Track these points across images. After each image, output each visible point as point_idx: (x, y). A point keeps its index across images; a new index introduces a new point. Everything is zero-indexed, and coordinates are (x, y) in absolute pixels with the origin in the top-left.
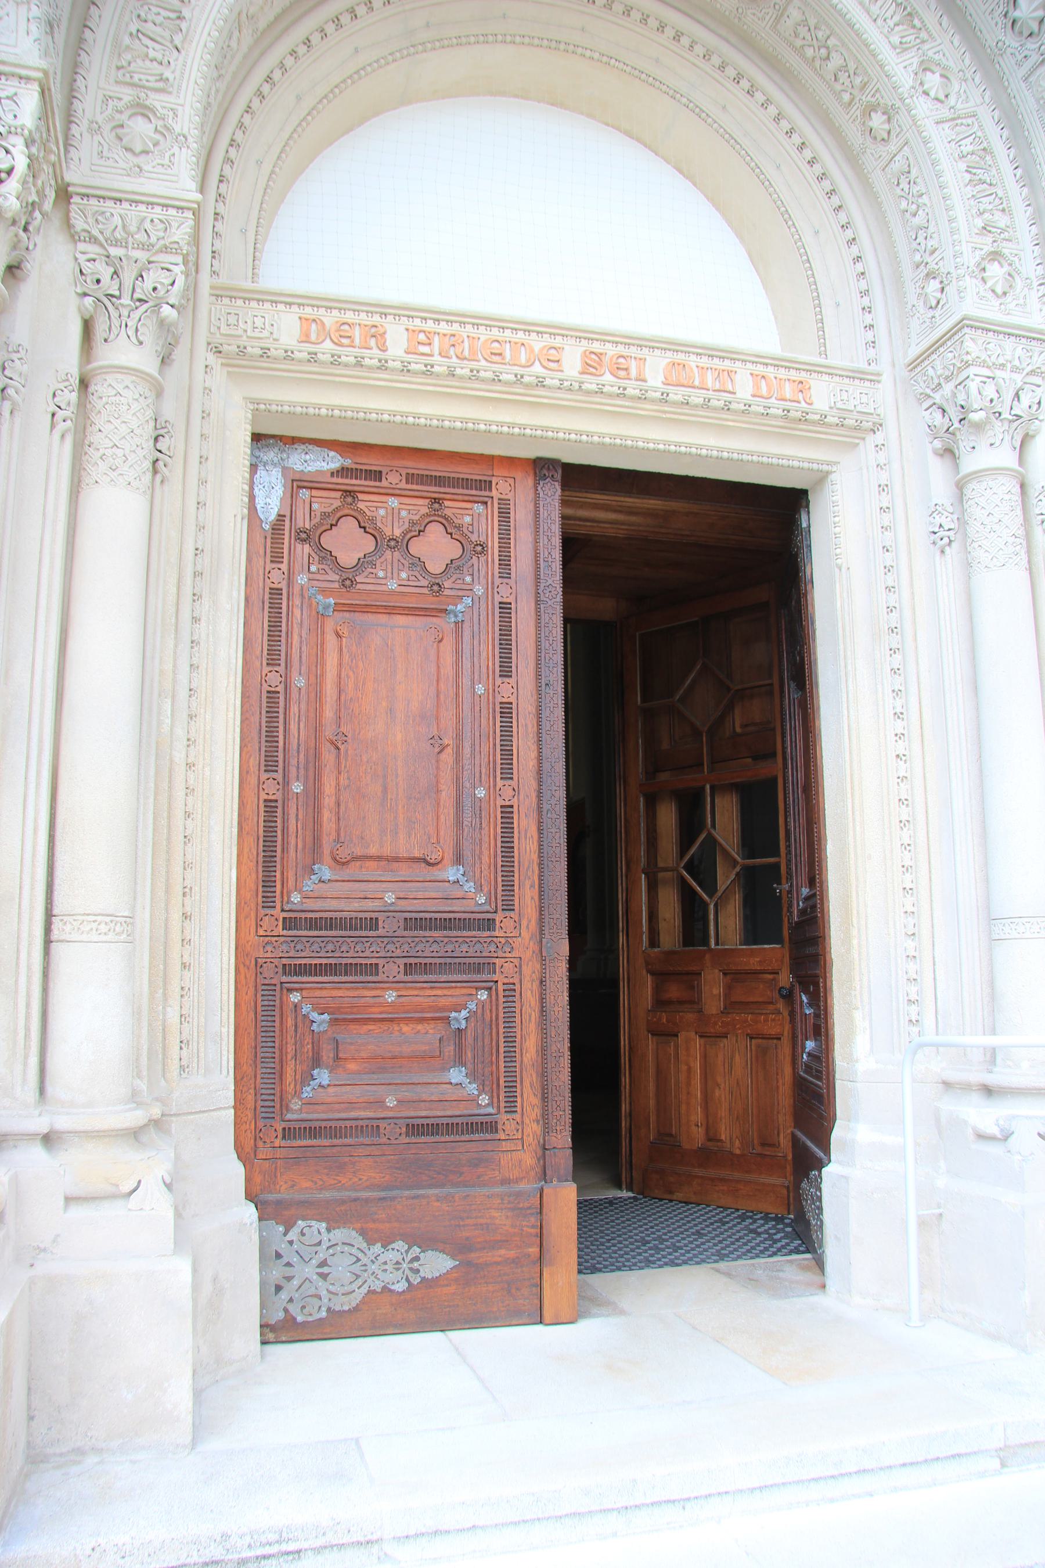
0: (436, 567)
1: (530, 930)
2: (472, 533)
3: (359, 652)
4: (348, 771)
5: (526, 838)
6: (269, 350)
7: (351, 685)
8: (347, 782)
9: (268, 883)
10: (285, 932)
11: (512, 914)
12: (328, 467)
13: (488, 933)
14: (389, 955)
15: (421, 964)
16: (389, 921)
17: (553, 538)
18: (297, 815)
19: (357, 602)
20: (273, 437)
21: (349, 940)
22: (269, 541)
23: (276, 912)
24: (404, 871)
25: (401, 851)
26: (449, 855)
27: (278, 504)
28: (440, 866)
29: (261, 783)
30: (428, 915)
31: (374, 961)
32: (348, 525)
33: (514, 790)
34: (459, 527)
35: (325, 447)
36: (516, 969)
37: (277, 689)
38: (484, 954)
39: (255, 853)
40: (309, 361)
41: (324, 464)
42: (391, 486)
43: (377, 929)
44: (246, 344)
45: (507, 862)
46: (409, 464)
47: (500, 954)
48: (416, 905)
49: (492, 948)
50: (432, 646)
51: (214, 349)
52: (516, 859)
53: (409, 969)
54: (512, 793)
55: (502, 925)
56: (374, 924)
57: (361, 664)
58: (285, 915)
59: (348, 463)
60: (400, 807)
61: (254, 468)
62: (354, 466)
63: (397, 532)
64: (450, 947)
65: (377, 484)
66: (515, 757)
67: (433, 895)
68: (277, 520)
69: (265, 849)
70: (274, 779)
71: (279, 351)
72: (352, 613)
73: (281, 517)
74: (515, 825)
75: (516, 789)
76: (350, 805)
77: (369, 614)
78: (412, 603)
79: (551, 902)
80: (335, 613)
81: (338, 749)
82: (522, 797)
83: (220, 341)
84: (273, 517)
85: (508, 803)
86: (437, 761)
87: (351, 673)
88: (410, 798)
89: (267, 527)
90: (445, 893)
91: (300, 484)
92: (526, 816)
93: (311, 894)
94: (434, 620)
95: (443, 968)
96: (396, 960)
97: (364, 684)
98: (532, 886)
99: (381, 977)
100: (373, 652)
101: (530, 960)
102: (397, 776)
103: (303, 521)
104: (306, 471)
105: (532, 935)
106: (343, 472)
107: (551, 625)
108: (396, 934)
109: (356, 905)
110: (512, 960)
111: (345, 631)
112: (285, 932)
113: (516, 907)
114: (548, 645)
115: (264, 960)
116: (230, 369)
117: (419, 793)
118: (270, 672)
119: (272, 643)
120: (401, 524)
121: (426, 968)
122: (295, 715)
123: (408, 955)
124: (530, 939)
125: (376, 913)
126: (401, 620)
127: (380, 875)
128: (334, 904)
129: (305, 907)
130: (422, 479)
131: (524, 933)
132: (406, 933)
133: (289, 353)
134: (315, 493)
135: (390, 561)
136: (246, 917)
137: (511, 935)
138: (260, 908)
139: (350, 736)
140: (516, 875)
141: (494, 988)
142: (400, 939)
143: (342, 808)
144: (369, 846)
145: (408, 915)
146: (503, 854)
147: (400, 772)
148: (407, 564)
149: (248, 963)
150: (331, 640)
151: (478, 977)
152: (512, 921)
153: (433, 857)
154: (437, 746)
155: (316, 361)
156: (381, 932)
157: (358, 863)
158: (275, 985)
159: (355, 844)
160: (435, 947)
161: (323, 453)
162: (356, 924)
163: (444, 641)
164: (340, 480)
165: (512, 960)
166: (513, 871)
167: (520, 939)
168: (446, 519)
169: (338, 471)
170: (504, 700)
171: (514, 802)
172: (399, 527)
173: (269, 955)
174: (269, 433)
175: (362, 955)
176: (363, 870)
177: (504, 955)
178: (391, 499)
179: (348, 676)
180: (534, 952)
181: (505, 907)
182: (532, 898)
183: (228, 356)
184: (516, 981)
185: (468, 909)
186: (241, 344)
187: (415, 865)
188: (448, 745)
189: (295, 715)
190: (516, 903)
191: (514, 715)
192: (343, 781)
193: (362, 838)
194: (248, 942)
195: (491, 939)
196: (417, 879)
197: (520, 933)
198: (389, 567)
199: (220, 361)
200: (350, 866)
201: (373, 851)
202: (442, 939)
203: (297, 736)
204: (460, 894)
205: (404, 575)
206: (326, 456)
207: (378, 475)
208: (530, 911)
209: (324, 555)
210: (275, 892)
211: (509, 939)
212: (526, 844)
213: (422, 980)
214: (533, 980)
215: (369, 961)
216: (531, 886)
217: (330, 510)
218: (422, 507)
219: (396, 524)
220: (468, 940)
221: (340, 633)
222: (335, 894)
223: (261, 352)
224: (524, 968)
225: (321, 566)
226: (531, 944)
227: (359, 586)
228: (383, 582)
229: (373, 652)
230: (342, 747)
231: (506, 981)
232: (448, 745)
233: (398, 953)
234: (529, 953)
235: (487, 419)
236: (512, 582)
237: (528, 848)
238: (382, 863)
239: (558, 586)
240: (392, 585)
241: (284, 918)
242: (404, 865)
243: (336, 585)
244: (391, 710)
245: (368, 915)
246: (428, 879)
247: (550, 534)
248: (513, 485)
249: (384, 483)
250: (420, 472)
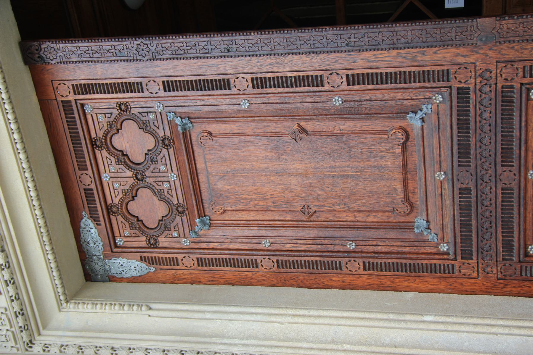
0: (150, 142)
1: (468, 54)
2: (111, 114)
3: (233, 197)
4: (333, 205)
5: (377, 61)
6: (16, 312)
7: (262, 203)
8: (342, 206)
9: (432, 269)
10: (474, 257)
11: (452, 72)
12: (94, 228)
13: (472, 96)
14: (493, 180)
15: (502, 153)
16: (462, 180)
17: (93, 48)
18: (374, 245)
19: (194, 201)
20: (83, 265)
21: (480, 211)
22: (162, 267)
23: (457, 264)
24: (415, 158)
25: (397, 163)
26: (399, 123)
27: (133, 261)
28: (408, 129)
29: (351, 272)
30: (455, 147)
31: (499, 191)
32: (134, 207)
33: (331, 74)
34: (110, 125)
35: (79, 231)
36: (509, 66)
37: (275, 261)
38: (493, 96)
39: (408, 278)
40: (14, 283)
41: (93, 231)
42: (93, 181)
43: (468, 88)
44: (17, 328)
45: (400, 78)
46: (71, 168)
47: (493, 81)
48: (446, 153)
49: (487, 89)
50: (216, 141)
51: (30, 345)
52: (397, 70)
53: (507, 162)
54: (334, 76)
55: (463, 81)
56: (464, 192)
57: (243, 196)
58: (459, 257)
59: (85, 214)
60: (359, 164)
61: (112, 279)
62: (87, 209)
63: (129, 173)
64: (486, 128)
65: (95, 191)
66: (302, 74)
67: (435, 140)
68: (146, 261)
69: (404, 270)
70: (347, 264)
71: (14, 306)
72: (204, 201)
73: (142, 259)
74: (365, 71)
75: (330, 72)
76: (361, 203)
77: (202, 189)
78: (184, 160)
79: (439, 39)
80: (206, 213)
81: (315, 212)
82: (337, 67)
83: (22, 344)
84: (144, 265)
85: (345, 79)
86: (315, 135)
87: (252, 203)
88: (350, 156)
89: (153, 269)
90: (434, 129)
91: (113, 247)
92: (354, 62)
93: (440, 236)
94: (194, 138)
95: (507, 133)
96: (498, 174)
97: (259, 193)
98: (423, 54)
99: (514, 185)
100: (232, 187)
101: (500, 52)
102: (331, 167)
103: (142, 241)
104: (102, 243)
105: (473, 52)
106: (94, 217)
107: (173, 49)
108: (474, 173)
109: (448, 202)
110: (499, 71)
111: (220, 208)
112: (474, 257)
113: (445, 68)
114: (192, 51)
115: (499, 273)
116: (41, 328)
117: (344, 149)
118: (262, 266)
119: (240, 264)
120: (121, 171)
121: (507, 148)
122: (293, 247)
123: (493, 164)
124: (477, 53)
125: (455, 189)
126: (200, 165)
127: (420, 180)
128: (448, 219)
129: (451, 240)
130: (80, 157)
131: (471, 59)
132: (473, 165)
133: (13, 298)
134: (117, 234)
135: (154, 179)
136: (462, 285)
137: (473, 72)
138: (454, 275)
139: (303, 204)
140: (413, 69)
141: (528, 86)
142: (478, 170)
143: (364, 208)
144: (395, 189)
145: (456, 164)
146: (393, 81)
147: (328, 165)
148: (152, 166)
149: (502, 285)
150: (226, 217)
151: (516, 104)
152: (459, 72)
153: (401, 137)
154: (301, 136)
155: (12, 279)
156: (472, 186)
157: (411, 195)
158: (521, 266)
159: (394, 199)
160: (486, 140)
161: (84, 232)
162: (465, 205)
163: (210, 130)
164: (101, 219)
165: (499, 71)
166: (410, 72)
167: (478, 63)
168: (107, 135)
169: (95, 220)
170: (251, 85)
171: (343, 73)
172: (125, 172)
173: (494, 270)
174: (81, 269)
175: (493, 202)
176: (416, 191)
177: (494, 78)
178: (104, 180)
179: (255, 206)
180: (491, 49)
181: (445, 78)
182: (435, 53)
183: (31, 335)
184: (521, 65)
185: (448, 112)
186: (18, 331)
187: (410, 150)
188: (299, 126)
189: (293, 247)
190: (440, 68)
191: (263, 76)
192: (342, 208)
193: (389, 194)
194: (484, 285)
195: (477, 91)
196: (422, 152)
197: (472, 63)
198: (159, 179)
199: (37, 338)
200: (413, 202)
201: (399, 186)
202: (478, 135)
203: (310, 246)
204: (434, 117)
205: (163, 168)
206: (86, 229)
207: (88, 192)
208: (448, 55)
209: (163, 226)
210: (440, 265)
211: (478, 74)
212: (382, 61)
213: (518, 152)
214: (521, 48)
215: (500, 196)
216: (423, 54)
217: (127, 224)
218: (102, 155)
219: (123, 175)
220: (479, 112)
221: (221, 211)
222: (439, 218)
223: (20, 316)
224: (507, 58)
225: (173, 229)
226: (483, 52)
227: (181, 201)
228: (172, 184)
229: (232, 187)
230: (314, 209)
231: (521, 75)
232: (299, 126)
233: (491, 172)
234: (492, 53)
235: (7, 135)
236: (144, 81)
237: (386, 59)
238: (409, 177)
239: (136, 43)
240: (173, 177)
241: (462, 258)
242: (410, 160)
243: (184, 218)
244: (277, 173)
245: (457, 196)
246: (421, 143)
247: (91, 52)
248: (59, 82)
249: (93, 186)
250: (75, 160)
